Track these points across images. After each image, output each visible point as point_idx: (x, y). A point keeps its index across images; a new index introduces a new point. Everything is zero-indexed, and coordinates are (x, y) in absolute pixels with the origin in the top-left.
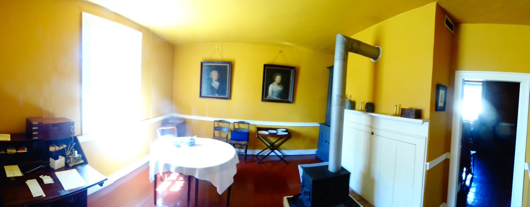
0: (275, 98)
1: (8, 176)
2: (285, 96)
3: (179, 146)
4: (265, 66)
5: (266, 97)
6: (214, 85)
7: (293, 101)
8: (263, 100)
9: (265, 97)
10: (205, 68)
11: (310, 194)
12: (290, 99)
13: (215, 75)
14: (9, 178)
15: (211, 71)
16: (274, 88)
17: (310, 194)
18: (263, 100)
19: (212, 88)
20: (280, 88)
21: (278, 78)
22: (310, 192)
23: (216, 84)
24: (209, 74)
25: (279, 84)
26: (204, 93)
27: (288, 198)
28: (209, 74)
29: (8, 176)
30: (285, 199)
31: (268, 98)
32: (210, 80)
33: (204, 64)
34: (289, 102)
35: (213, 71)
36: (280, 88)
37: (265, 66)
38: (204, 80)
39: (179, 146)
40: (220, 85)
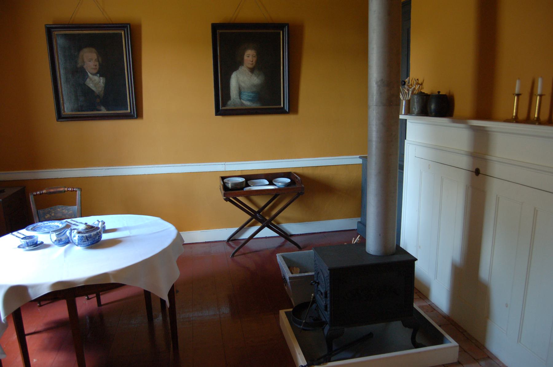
0: (248, 104)
1: (280, 311)
2: (274, 99)
3: (507, 306)
4: (215, 27)
5: (224, 104)
6: (91, 85)
7: (293, 109)
8: (219, 112)
9: (223, 106)
10: (59, 42)
11: (326, 297)
12: (284, 103)
13: (90, 59)
14: (279, 313)
15: (80, 49)
16: (243, 81)
17: (326, 297)
18: (219, 112)
19: (88, 92)
20: (255, 80)
21: (250, 56)
22: (326, 293)
23: (96, 83)
24: (72, 57)
25: (252, 70)
26: (67, 108)
27: (286, 313)
28: (72, 57)
29: (280, 311)
30: (282, 313)
31: (231, 105)
32: (78, 73)
33: (56, 33)
34: (281, 111)
35: (85, 50)
36: (255, 80)
37: (215, 27)
38: (61, 72)
39: (507, 306)
40: (107, 84)
